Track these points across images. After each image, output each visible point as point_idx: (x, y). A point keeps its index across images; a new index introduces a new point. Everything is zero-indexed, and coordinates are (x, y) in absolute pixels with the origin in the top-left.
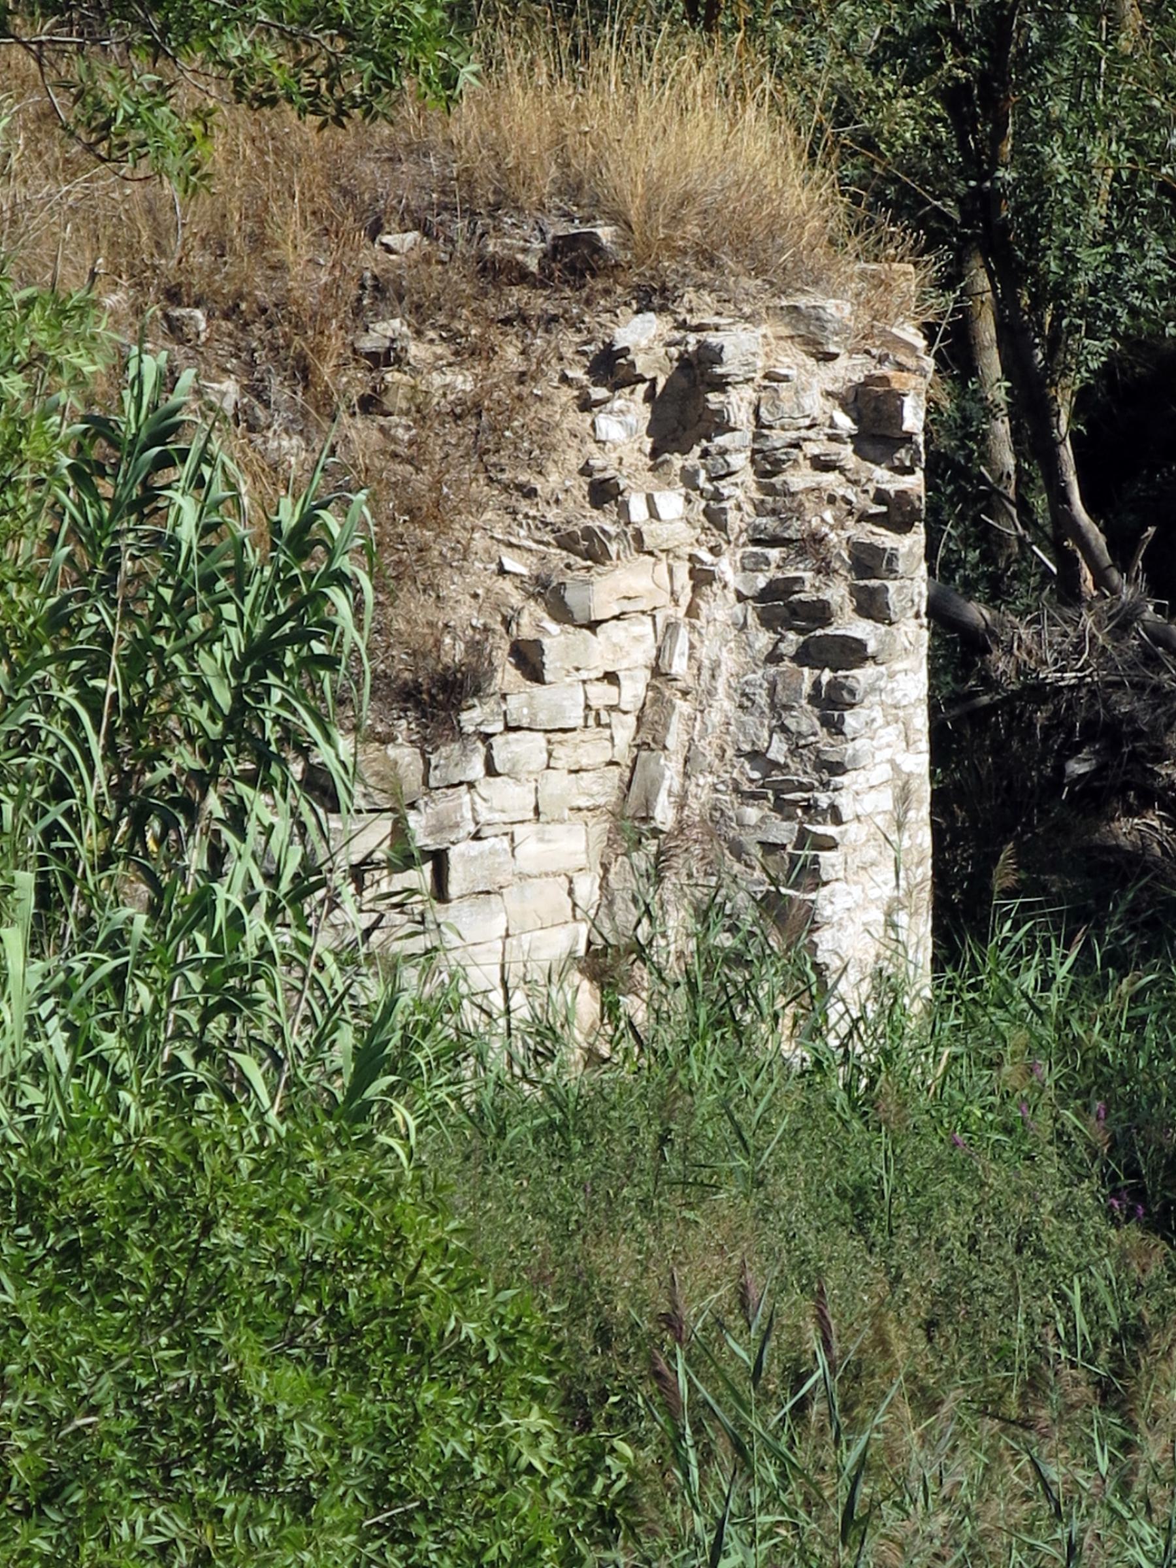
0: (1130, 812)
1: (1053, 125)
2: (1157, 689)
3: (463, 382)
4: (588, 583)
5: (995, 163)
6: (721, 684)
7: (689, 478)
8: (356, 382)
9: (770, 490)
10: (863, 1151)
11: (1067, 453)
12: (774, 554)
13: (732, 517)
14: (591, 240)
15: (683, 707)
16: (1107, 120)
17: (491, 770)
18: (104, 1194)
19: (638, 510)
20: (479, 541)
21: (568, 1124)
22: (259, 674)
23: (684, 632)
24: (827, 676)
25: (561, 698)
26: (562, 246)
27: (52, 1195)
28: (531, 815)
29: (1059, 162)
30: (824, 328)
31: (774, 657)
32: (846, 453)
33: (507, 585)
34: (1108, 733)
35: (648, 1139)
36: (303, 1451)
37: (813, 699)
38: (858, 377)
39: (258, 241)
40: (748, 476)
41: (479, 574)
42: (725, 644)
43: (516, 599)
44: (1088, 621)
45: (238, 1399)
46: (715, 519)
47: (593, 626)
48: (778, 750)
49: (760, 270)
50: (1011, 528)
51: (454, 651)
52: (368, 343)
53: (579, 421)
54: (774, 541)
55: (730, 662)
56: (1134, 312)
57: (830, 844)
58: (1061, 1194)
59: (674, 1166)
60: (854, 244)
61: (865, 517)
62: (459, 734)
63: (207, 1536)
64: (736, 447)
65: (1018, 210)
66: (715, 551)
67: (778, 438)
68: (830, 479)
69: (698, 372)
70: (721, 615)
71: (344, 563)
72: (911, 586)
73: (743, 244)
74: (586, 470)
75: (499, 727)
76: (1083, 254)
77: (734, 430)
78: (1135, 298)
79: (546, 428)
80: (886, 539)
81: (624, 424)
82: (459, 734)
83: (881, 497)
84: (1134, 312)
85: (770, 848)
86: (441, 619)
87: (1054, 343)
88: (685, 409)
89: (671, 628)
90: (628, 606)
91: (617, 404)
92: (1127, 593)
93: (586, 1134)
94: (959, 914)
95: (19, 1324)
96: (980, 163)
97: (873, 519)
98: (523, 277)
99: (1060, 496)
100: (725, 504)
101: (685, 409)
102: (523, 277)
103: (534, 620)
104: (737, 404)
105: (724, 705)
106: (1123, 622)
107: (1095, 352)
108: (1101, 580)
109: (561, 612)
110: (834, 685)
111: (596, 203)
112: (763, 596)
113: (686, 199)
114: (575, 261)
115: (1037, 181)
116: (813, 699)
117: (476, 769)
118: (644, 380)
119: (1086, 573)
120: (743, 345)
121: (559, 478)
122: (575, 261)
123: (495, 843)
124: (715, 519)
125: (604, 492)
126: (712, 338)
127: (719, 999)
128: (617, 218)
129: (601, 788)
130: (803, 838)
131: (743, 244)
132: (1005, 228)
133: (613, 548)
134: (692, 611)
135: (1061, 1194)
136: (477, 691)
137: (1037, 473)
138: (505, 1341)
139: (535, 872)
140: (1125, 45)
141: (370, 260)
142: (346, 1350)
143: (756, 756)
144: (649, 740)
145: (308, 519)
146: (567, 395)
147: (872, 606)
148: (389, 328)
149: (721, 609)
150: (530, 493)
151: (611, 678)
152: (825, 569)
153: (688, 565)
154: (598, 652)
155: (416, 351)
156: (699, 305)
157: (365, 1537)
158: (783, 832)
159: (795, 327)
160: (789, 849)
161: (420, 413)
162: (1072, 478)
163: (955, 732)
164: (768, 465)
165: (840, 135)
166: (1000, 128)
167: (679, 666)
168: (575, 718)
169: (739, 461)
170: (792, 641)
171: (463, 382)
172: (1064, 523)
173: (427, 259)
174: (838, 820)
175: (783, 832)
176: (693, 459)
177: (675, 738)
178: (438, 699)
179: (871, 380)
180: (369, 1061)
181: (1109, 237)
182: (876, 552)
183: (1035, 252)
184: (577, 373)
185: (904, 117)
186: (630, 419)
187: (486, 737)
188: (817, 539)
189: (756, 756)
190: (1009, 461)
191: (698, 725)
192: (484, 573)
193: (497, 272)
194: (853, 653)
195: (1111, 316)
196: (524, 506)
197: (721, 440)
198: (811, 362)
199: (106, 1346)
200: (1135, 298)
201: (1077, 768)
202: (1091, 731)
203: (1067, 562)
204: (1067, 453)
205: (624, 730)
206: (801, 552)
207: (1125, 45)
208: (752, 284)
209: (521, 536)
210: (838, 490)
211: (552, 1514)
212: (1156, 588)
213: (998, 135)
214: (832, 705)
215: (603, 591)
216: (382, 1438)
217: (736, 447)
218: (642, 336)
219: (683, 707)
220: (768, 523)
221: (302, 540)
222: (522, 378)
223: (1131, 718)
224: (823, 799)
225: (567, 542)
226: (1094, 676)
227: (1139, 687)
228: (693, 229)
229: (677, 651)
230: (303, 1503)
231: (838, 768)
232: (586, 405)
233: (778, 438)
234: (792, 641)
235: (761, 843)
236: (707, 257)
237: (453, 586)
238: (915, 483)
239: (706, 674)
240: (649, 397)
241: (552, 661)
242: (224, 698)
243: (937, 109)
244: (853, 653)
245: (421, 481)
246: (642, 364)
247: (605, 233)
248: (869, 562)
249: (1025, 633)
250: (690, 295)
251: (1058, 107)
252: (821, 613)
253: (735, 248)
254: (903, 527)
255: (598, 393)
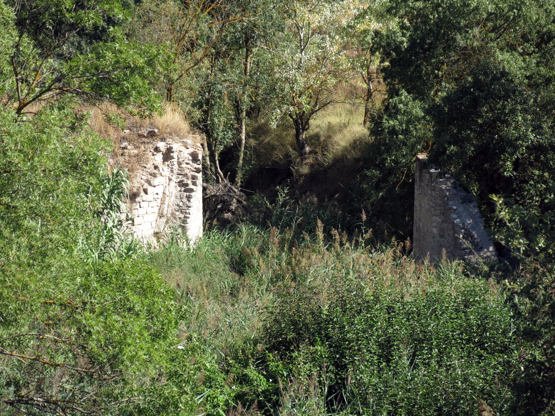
0: (226, 213)
1: (216, 115)
2: (230, 196)
3: (136, 151)
5: (207, 121)
6: (173, 195)
7: (168, 165)
8: (120, 151)
9: (180, 167)
10: (196, 262)
11: (217, 162)
12: (180, 176)
13: (175, 171)
14: (154, 132)
16: (223, 114)
17: (140, 207)
18: (109, 270)
19: (161, 170)
20: (138, 174)
21: (153, 258)
22: (111, 194)
23: (168, 188)
24: (188, 194)
25: (149, 197)
26: (150, 132)
27: (102, 271)
29: (216, 120)
31: (180, 191)
32: (190, 162)
33: (142, 180)
34: (223, 202)
35: (165, 260)
36: (137, 308)
37: (186, 197)
38: (192, 151)
39: (106, 131)
40: (176, 165)
41: (138, 179)
42: (174, 189)
43: (144, 182)
44: (220, 186)
45: (128, 300)
46: (172, 171)
47: (155, 186)
48: (181, 204)
49: (178, 136)
50: (209, 173)
51: (135, 190)
52: (122, 146)
53: (153, 157)
54: (180, 175)
56: (227, 142)
57: (188, 218)
58: (223, 268)
59: (169, 264)
60: (191, 133)
61: (193, 171)
62: (136, 202)
63: (124, 320)
64: (175, 161)
65: (211, 127)
66: (172, 176)
67: (181, 160)
68: (188, 166)
69: (169, 150)
71: (124, 179)
72: (200, 181)
73: (175, 132)
74: (153, 164)
76: (220, 134)
78: (227, 140)
79: (148, 158)
80: (196, 174)
81: (159, 157)
82: (136, 202)
83: (195, 168)
84: (227, 142)
85: (180, 218)
86: (133, 185)
87: (215, 146)
88: (168, 156)
89: (166, 187)
92: (226, 182)
93: (156, 259)
94: (208, 227)
95: (97, 289)
96: (205, 120)
97: (195, 171)
98: (144, 137)
99: (216, 168)
101: (168, 156)
102: (144, 137)
103: (146, 186)
104: (175, 155)
105: (173, 198)
106: (225, 186)
107: (222, 148)
108: (222, 180)
109: (150, 184)
110: (189, 195)
111: (155, 126)
112: (179, 182)
113: (168, 126)
114: (152, 134)
115: (213, 124)
116: (186, 197)
117: (138, 207)
119: (220, 179)
120: (176, 146)
121: (150, 165)
122: (152, 134)
123: (141, 218)
124: (172, 171)
125: (156, 167)
126: (171, 145)
127: (173, 241)
128: (157, 128)
129: (156, 210)
130: (185, 217)
131: (175, 132)
132: (209, 130)
133: (157, 175)
134: (169, 185)
135: (223, 268)
136: (138, 196)
137: (213, 164)
138: (167, 292)
140: (225, 104)
141: (122, 134)
142: (143, 293)
143: (178, 205)
144: (163, 203)
145: (118, 172)
146: (151, 154)
147: (194, 184)
148: (125, 144)
149: (173, 184)
150: (145, 167)
151: (157, 194)
152: (188, 179)
154: (155, 190)
155: (129, 147)
156: (169, 141)
157: (147, 320)
158: (182, 216)
161: (130, 156)
162: (218, 165)
163: (206, 201)
164: (179, 164)
165: (188, 115)
166: (208, 116)
167: (167, 192)
168: (152, 199)
169: (176, 163)
170: (183, 189)
171: (136, 151)
172: (217, 172)
173: (130, 134)
174: (190, 214)
175: (182, 216)
176: (169, 163)
177: (166, 202)
178: (134, 196)
179: (194, 152)
180: (129, 249)
181: (223, 131)
182: (195, 176)
183: (213, 133)
184: (152, 150)
185: (197, 114)
187: (139, 202)
188: (187, 174)
189: (178, 205)
190: (209, 163)
192: (138, 180)
193: (141, 136)
194: (192, 190)
195: (224, 143)
196: (145, 169)
197: (173, 160)
199: (109, 293)
200: (227, 140)
201: (219, 207)
202: (221, 201)
203: (217, 177)
204: (217, 162)
205: (159, 201)
206: (184, 176)
207: (225, 104)
208: (177, 138)
209: (144, 174)
210: (190, 168)
211: (173, 316)
212: (230, 181)
213: (208, 117)
214: (189, 198)
215: (155, 182)
216: (149, 306)
217: (175, 161)
218: (162, 145)
219: (167, 198)
220: (180, 172)
221: (118, 174)
222: (144, 151)
223: (227, 200)
224: (188, 211)
225: (151, 175)
226: (221, 194)
227: (228, 195)
228: (168, 130)
230: (138, 315)
231: (189, 207)
232: (153, 155)
233: (181, 160)
234: (183, 189)
236: (170, 134)
237: (135, 181)
238: (200, 166)
240: (163, 154)
241: (149, 192)
242: (106, 197)
243: (202, 113)
244: (192, 190)
245: (130, 166)
246: (162, 149)
247: (156, 130)
248: (194, 178)
249: (212, 187)
250: (168, 139)
251: (216, 113)
252: (187, 185)
253: (175, 133)
254: (198, 172)
255: (155, 153)
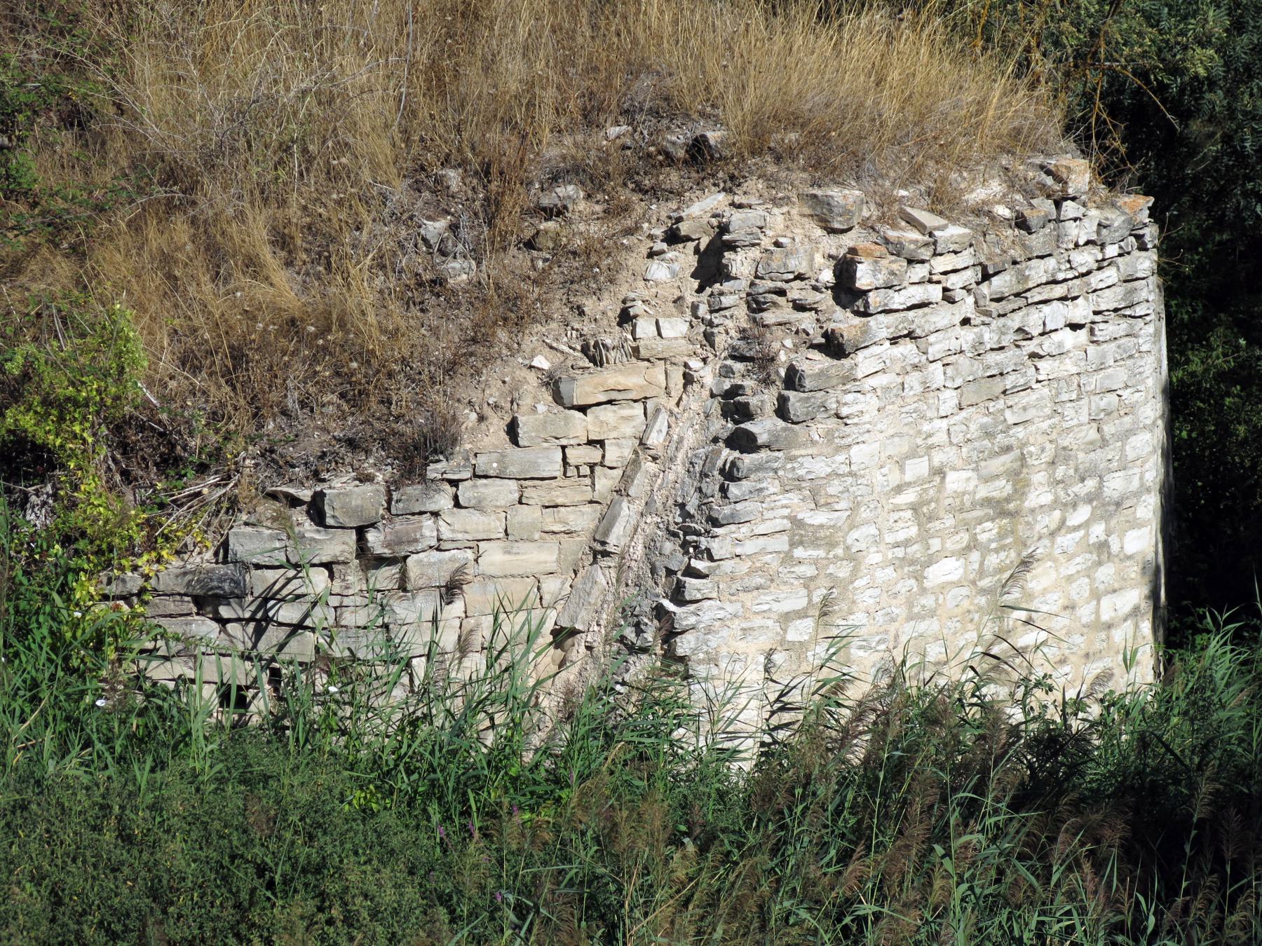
4: (574, 379)
6: (681, 455)
15: (651, 467)
17: (457, 505)
28: (502, 535)
30: (831, 211)
54: (741, 358)
55: (691, 438)
62: (423, 479)
70: (695, 406)
75: (467, 474)
77: (736, 278)
90: (614, 395)
91: (670, 255)
100: (715, 330)
105: (679, 468)
118: (693, 240)
129: (583, 520)
139: (500, 574)
149: (697, 401)
153: (682, 369)
159: (814, 209)
160: (679, 574)
186: (676, 266)
191: (659, 481)
198: (819, 232)
229: (656, 427)
235: (667, 568)
239: (673, 445)
